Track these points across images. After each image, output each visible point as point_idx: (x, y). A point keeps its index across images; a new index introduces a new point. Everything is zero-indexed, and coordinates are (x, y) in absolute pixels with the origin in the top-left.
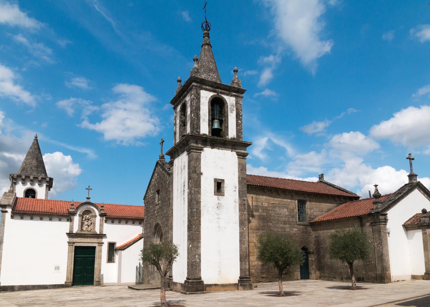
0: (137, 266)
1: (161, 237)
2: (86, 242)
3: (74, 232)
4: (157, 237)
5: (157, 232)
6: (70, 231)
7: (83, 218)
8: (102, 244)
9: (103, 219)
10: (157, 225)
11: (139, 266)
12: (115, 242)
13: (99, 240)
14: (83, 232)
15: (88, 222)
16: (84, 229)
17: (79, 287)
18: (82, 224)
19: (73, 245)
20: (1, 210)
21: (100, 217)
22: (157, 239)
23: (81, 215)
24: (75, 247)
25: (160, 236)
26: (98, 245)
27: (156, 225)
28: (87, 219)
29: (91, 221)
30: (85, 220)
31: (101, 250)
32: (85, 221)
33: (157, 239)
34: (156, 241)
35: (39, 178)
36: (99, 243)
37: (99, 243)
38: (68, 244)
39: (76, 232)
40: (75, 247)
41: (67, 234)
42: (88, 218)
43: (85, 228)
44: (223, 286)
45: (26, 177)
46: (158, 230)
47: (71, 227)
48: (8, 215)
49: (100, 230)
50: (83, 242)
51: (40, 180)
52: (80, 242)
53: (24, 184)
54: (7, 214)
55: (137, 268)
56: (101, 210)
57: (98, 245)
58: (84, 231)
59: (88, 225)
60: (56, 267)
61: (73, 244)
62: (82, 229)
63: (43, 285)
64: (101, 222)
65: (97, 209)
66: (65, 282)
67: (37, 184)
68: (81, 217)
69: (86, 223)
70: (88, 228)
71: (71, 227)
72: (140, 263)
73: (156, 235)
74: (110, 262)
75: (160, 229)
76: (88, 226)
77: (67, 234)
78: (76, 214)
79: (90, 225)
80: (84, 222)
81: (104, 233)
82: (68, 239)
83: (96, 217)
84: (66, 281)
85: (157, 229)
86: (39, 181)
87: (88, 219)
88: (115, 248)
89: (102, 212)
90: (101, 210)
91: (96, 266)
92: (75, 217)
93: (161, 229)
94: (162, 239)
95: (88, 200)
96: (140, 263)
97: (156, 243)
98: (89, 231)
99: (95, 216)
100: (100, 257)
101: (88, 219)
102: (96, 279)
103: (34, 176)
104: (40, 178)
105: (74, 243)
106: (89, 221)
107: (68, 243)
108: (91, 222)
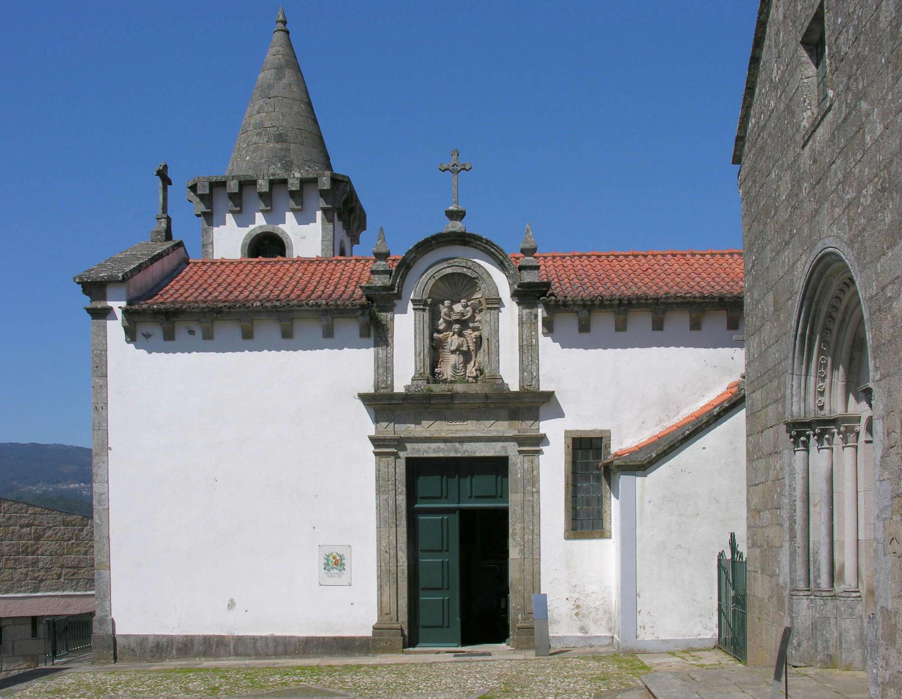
0: (721, 554)
1: (851, 360)
2: (470, 434)
3: (399, 387)
4: (825, 365)
5: (826, 329)
6: (377, 386)
7: (435, 316)
8: (538, 445)
9: (536, 316)
10: (821, 274)
11: (728, 555)
12: (602, 431)
13: (523, 427)
14: (438, 389)
15: (460, 335)
16: (446, 370)
17: (438, 653)
18: (435, 350)
19: (397, 456)
20: (89, 305)
21: (518, 304)
22: (827, 380)
23: (425, 304)
24: (409, 461)
25: (844, 355)
26: (520, 452)
27: (815, 275)
28: (457, 321)
29: (475, 329)
30: (449, 324)
31: (535, 473)
32: (445, 330)
33: (823, 379)
34: (822, 393)
35: (290, 181)
36: (521, 441)
37: (521, 441)
38: (372, 448)
39: (407, 388)
40: (409, 461)
41: (364, 397)
42: (463, 315)
43: (449, 364)
44: (832, 487)
45: (272, 183)
46: (830, 317)
47: (384, 368)
48: (115, 328)
49: (522, 370)
50: (443, 435)
51: (294, 189)
52: (427, 435)
53: (243, 219)
54: (110, 323)
55: (720, 566)
56: (521, 268)
57: (520, 452)
58: (445, 381)
59: (465, 348)
60: (331, 558)
61: (395, 447)
62: (433, 374)
63: (276, 640)
64: (712, 421)
65: (502, 265)
66: (374, 628)
67: (290, 216)
68: (424, 310)
69: (454, 341)
70: (466, 368)
71: (384, 368)
72: (733, 536)
73: (821, 352)
74: (576, 537)
75: (844, 304)
76: (461, 359)
77: (364, 397)
78: (399, 296)
79: (472, 348)
80: (440, 336)
81: (544, 388)
82: (373, 426)
83: (498, 308)
84: (379, 626)
85: (824, 308)
86: (292, 194)
87: (464, 323)
88: (604, 461)
89: (529, 277)
90: (521, 268)
91: (514, 553)
92: (399, 319)
93: (856, 293)
94: (824, 58)
95: (456, 226)
96: (733, 536)
97: (821, 408)
98: (470, 379)
99: (496, 304)
100: (535, 513)
101: (464, 323)
102: (515, 617)
103: (272, 178)
104: (294, 185)
105: (400, 443)
106: (468, 332)
107: (376, 446)
108: (477, 333)
